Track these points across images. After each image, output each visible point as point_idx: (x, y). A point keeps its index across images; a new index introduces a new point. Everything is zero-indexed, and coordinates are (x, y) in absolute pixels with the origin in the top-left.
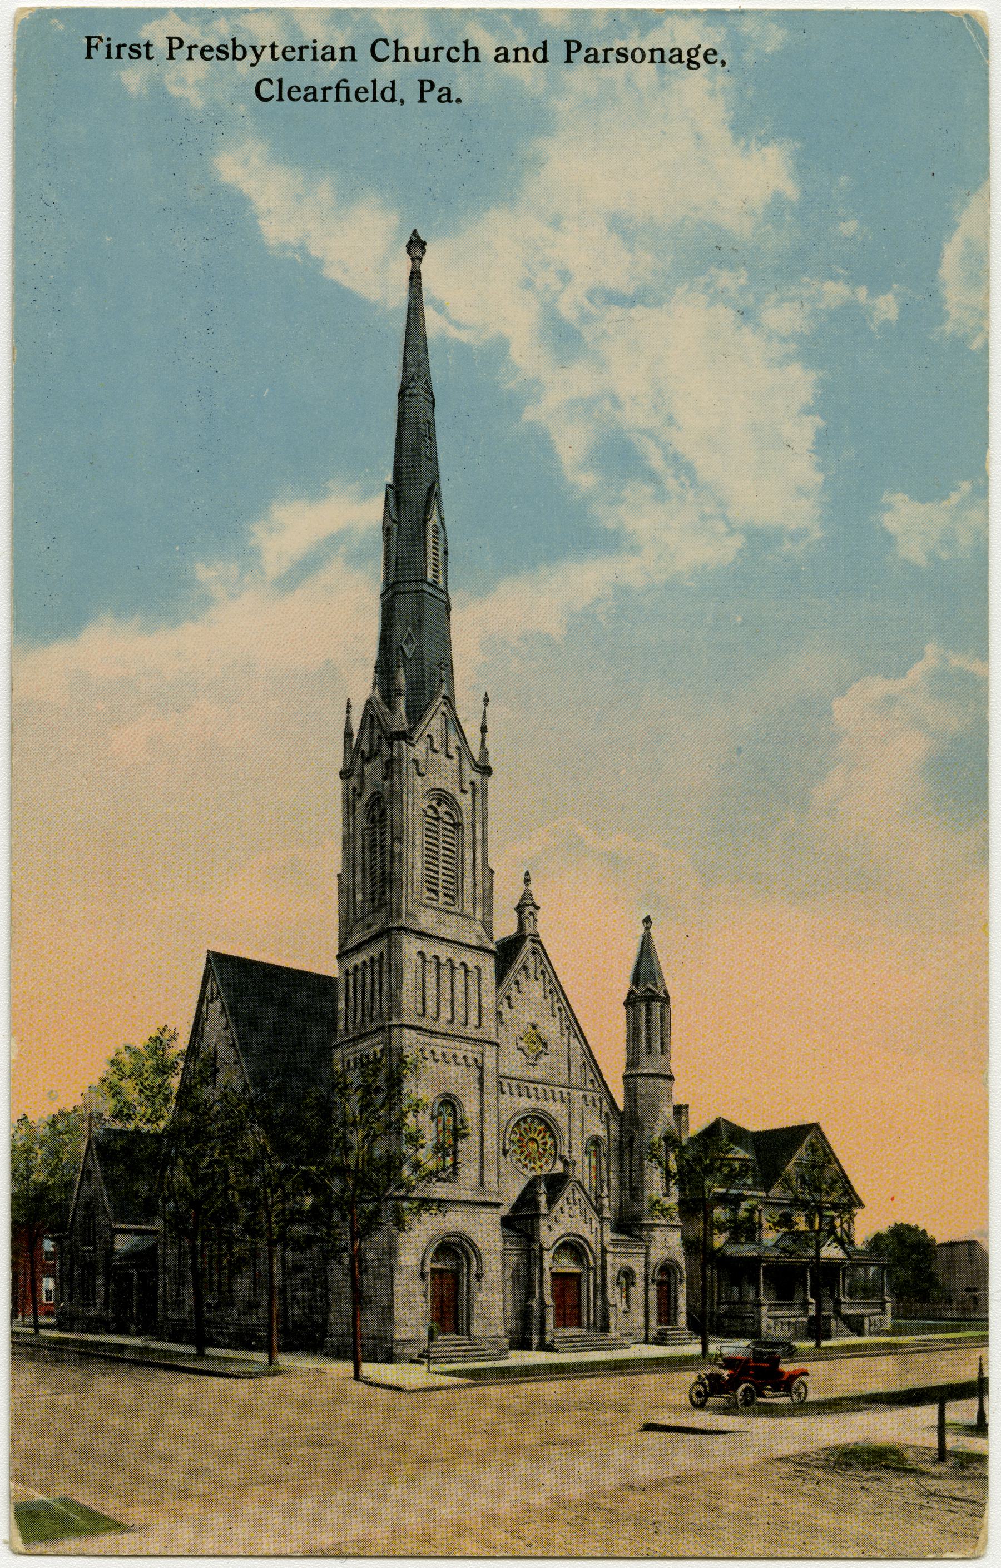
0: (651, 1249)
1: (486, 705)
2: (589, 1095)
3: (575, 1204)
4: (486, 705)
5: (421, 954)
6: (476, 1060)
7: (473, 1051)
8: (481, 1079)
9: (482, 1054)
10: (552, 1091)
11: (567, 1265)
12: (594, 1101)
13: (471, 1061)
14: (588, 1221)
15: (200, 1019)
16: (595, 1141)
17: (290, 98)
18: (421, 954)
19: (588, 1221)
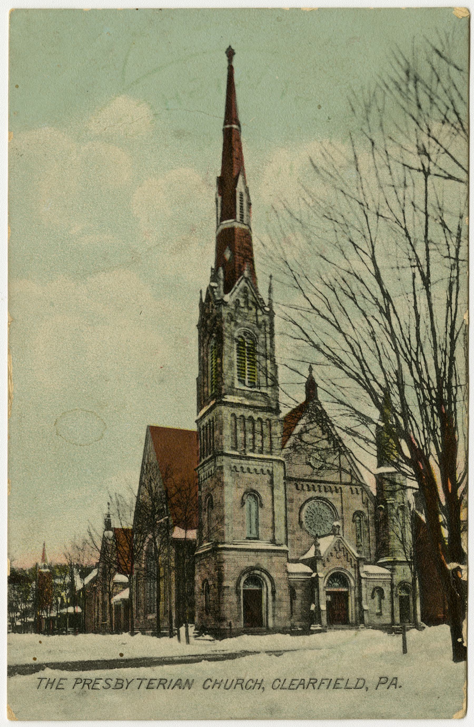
0: (394, 576)
1: (271, 279)
2: (353, 488)
3: (340, 550)
4: (271, 279)
5: (233, 415)
6: (268, 471)
7: (266, 466)
8: (271, 482)
9: (272, 468)
10: (313, 485)
11: (337, 588)
12: (336, 489)
13: (265, 471)
14: (349, 560)
15: (387, 569)
16: (358, 513)
17: (81, 680)
18: (233, 415)
19: (349, 560)
